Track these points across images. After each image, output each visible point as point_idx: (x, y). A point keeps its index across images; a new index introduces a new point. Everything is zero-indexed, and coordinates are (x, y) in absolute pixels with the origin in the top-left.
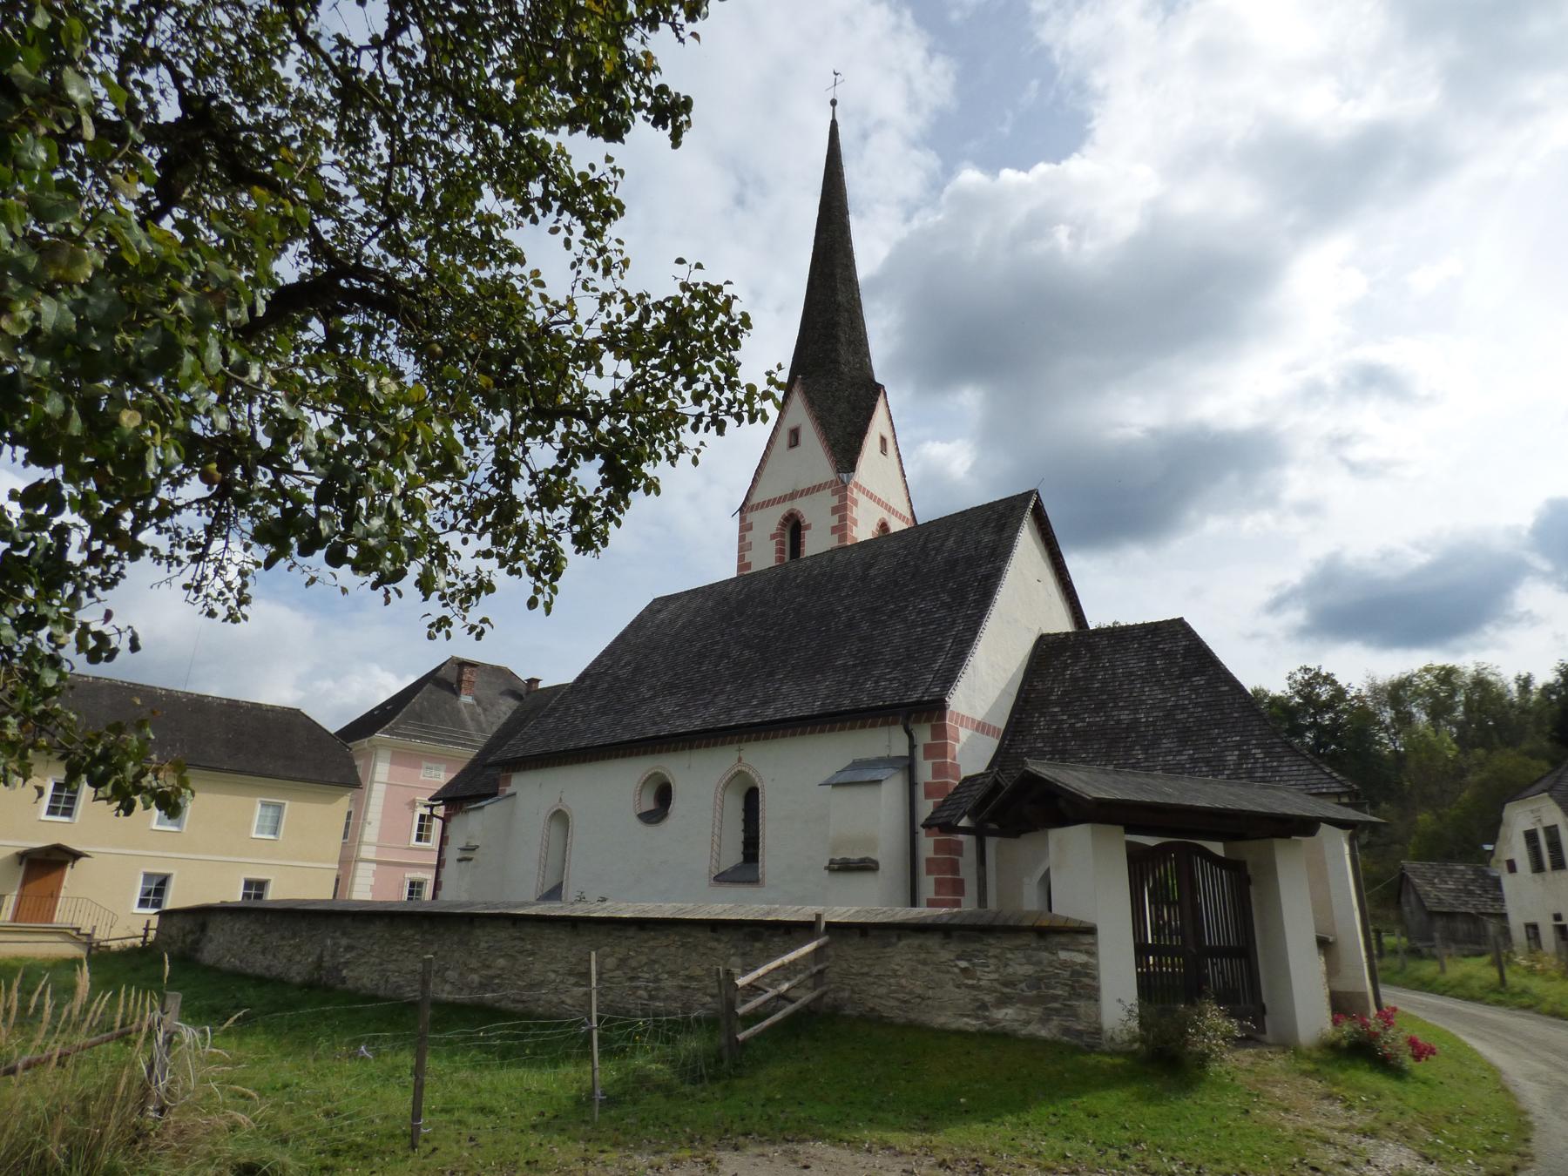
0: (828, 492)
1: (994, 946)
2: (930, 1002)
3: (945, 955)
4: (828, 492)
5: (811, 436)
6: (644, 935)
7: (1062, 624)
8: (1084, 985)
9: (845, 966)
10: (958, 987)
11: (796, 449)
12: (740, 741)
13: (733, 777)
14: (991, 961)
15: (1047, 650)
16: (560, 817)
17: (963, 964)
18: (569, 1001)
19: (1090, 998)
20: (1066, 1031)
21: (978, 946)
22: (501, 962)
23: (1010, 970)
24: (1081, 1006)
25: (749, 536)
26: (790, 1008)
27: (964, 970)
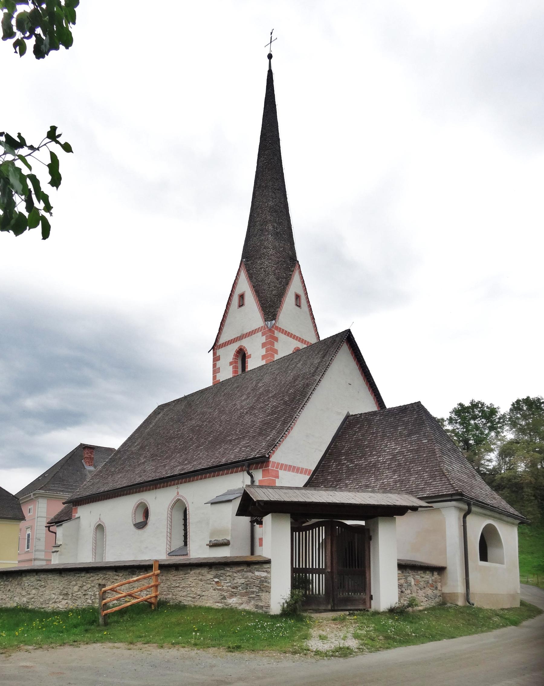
0: (260, 333)
1: (229, 571)
2: (203, 597)
3: (209, 576)
4: (260, 333)
5: (251, 299)
6: (88, 575)
7: (367, 406)
8: (264, 586)
9: (169, 584)
10: (214, 590)
11: (243, 308)
12: (178, 484)
13: (175, 504)
14: (228, 578)
15: (350, 423)
16: (100, 528)
17: (216, 580)
18: (61, 607)
19: (267, 592)
20: (257, 606)
21: (222, 571)
22: (34, 591)
23: (235, 581)
24: (263, 595)
25: (219, 364)
26: (134, 601)
27: (217, 582)
